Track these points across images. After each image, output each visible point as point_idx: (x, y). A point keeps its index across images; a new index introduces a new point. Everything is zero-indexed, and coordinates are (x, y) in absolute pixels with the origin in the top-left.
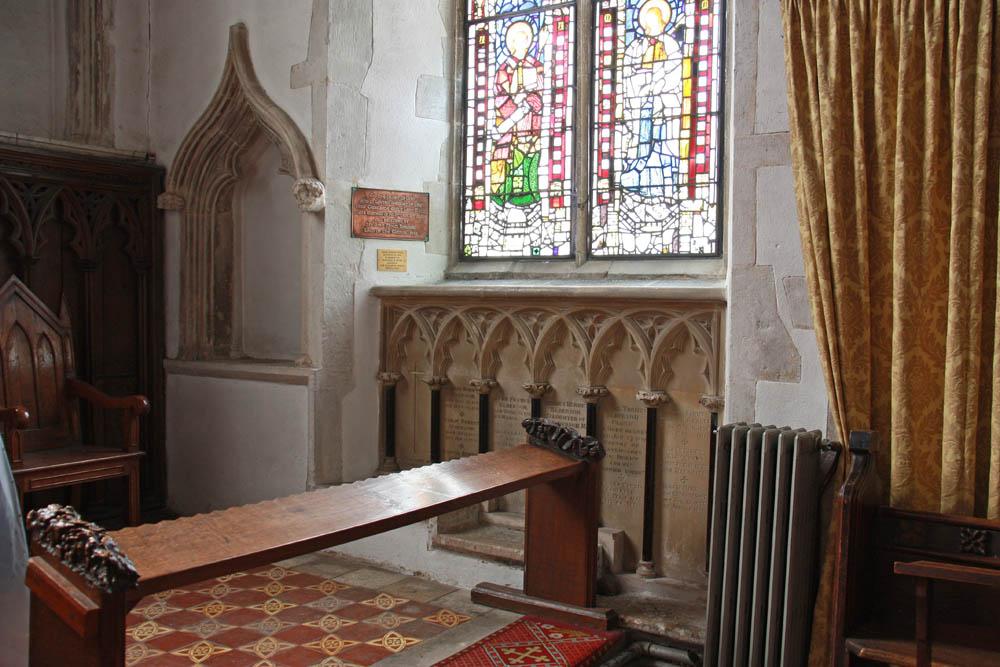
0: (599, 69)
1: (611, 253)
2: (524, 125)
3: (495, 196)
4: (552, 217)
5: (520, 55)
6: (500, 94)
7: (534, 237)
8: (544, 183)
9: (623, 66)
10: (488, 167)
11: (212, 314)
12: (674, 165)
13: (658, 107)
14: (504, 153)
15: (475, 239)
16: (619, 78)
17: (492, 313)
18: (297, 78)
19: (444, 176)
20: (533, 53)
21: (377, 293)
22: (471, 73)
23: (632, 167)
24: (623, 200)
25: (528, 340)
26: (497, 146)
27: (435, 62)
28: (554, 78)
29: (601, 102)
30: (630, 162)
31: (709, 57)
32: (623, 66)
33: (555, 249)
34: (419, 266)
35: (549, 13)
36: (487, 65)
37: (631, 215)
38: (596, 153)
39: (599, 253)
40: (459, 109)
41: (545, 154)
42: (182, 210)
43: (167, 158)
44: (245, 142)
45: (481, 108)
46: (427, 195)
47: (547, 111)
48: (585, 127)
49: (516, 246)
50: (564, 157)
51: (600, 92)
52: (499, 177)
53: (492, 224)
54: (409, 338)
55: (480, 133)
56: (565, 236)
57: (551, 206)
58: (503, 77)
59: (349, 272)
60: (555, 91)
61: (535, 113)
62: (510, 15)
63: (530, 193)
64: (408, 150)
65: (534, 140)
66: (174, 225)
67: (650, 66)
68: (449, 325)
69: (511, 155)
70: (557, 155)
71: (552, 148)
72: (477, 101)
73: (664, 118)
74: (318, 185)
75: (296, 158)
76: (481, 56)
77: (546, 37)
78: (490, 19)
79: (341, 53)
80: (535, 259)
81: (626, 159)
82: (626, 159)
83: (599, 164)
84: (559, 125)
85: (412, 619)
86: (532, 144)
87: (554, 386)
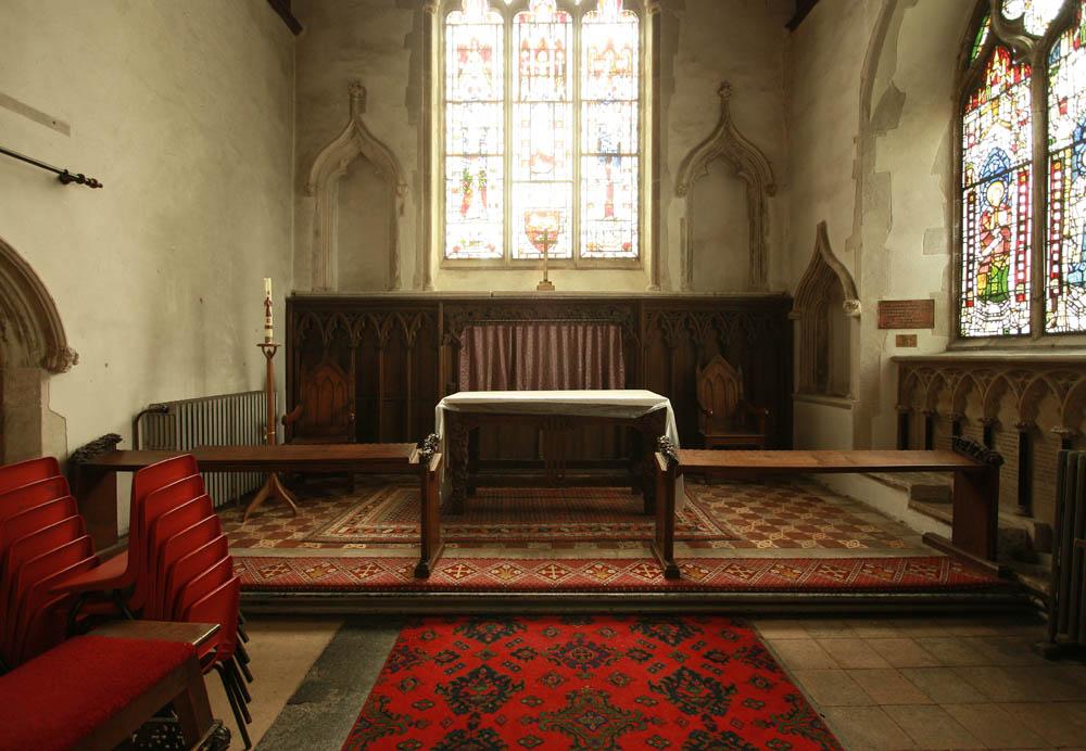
1: (1060, 330)
2: (999, 249)
3: (980, 297)
4: (1018, 308)
5: (996, 204)
6: (983, 231)
7: (1005, 322)
8: (1011, 286)
10: (975, 280)
14: (986, 269)
15: (967, 325)
16: (1066, 206)
17: (960, 373)
18: (849, 245)
19: (947, 288)
21: (894, 360)
22: (965, 221)
24: (1069, 293)
25: (980, 393)
26: (982, 265)
27: (939, 220)
28: (1019, 214)
29: (1052, 225)
33: (1020, 330)
34: (929, 343)
35: (1015, 171)
36: (975, 214)
37: (1076, 302)
38: (1048, 262)
39: (1051, 331)
40: (956, 244)
41: (1012, 267)
42: (801, 318)
43: (793, 294)
44: (828, 286)
45: (971, 242)
46: (933, 301)
47: (1014, 238)
48: (1040, 244)
49: (993, 328)
50: (1025, 267)
51: (1052, 219)
52: (983, 285)
53: (979, 315)
54: (915, 386)
55: (971, 258)
56: (1026, 321)
57: (1017, 300)
58: (985, 220)
59: (877, 348)
60: (1019, 223)
61: (1006, 240)
62: (989, 179)
63: (1003, 293)
64: (918, 271)
66: (797, 327)
68: (935, 378)
69: (990, 270)
70: (1021, 266)
71: (1017, 262)
72: (969, 238)
74: (857, 302)
75: (845, 289)
76: (971, 209)
77: (1013, 189)
78: (976, 184)
79: (870, 228)
80: (1006, 336)
81: (1071, 264)
82: (1071, 264)
83: (1051, 269)
84: (1022, 246)
85: (941, 554)
86: (1004, 261)
87: (1001, 420)
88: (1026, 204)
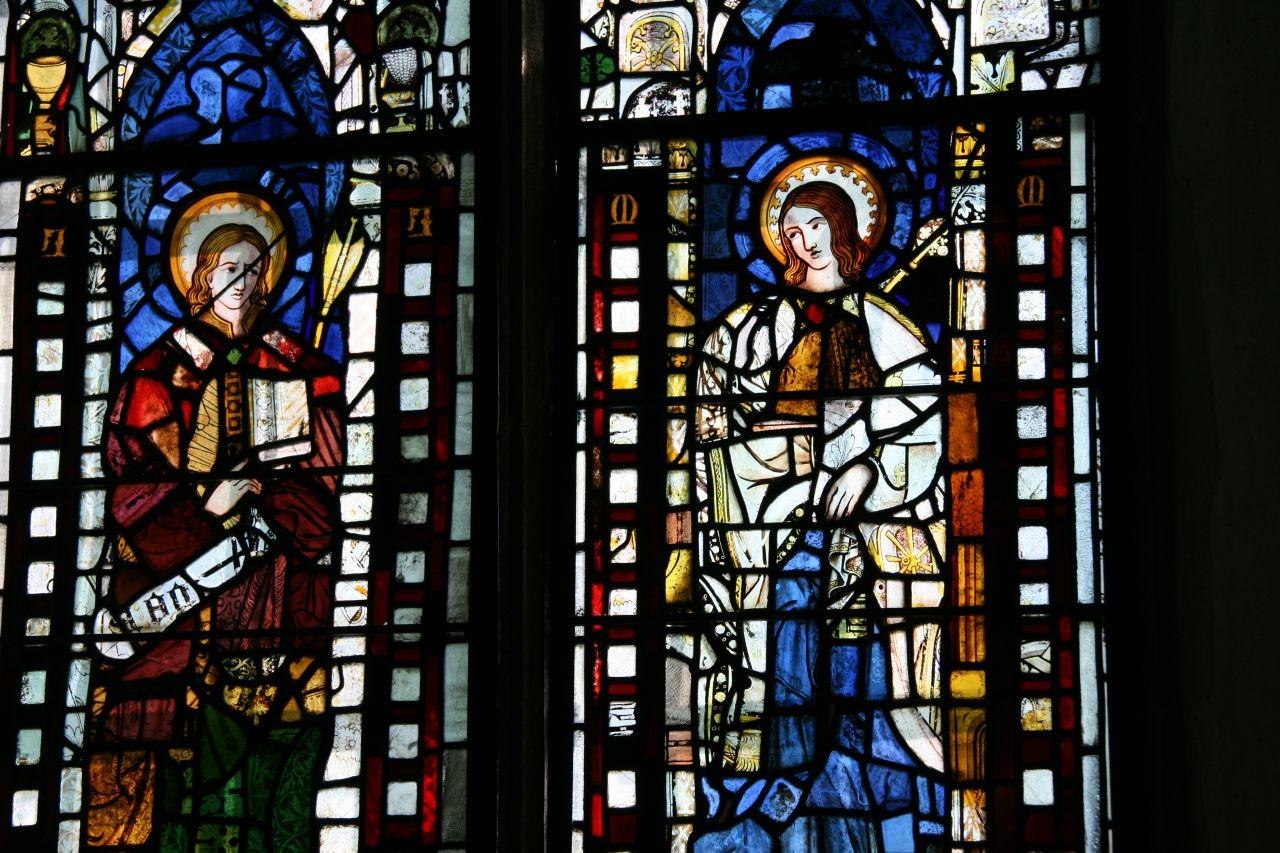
0: (589, 404)
9: (692, 400)
11: (709, 717)
12: (924, 805)
13: (847, 566)
20: (293, 317)
23: (743, 806)
30: (732, 785)
31: (1052, 392)
32: (692, 400)
41: (348, 734)
58: (150, 408)
65: (296, 671)
67: (806, 409)
73: (874, 614)
88: (436, 366)
